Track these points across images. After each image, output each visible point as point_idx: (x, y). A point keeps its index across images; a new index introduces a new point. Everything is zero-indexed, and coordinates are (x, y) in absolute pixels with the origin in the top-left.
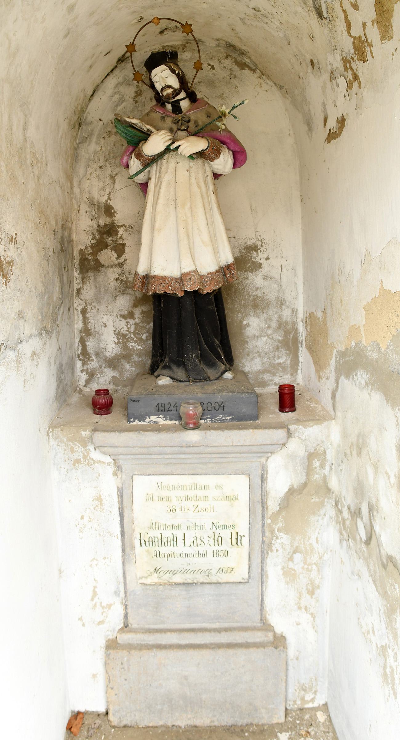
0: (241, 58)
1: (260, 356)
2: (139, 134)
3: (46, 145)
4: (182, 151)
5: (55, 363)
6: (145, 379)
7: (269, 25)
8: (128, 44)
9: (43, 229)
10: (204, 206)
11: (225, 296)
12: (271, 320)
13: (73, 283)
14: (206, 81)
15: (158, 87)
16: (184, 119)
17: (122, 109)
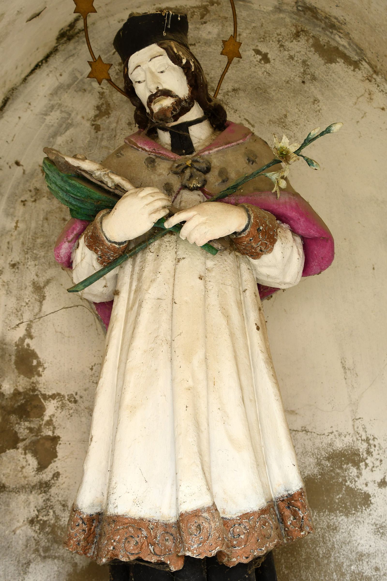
0: (327, 35)
2: (97, 194)
4: (190, 234)
10: (236, 357)
14: (250, 87)
16: (196, 165)
17: (67, 142)
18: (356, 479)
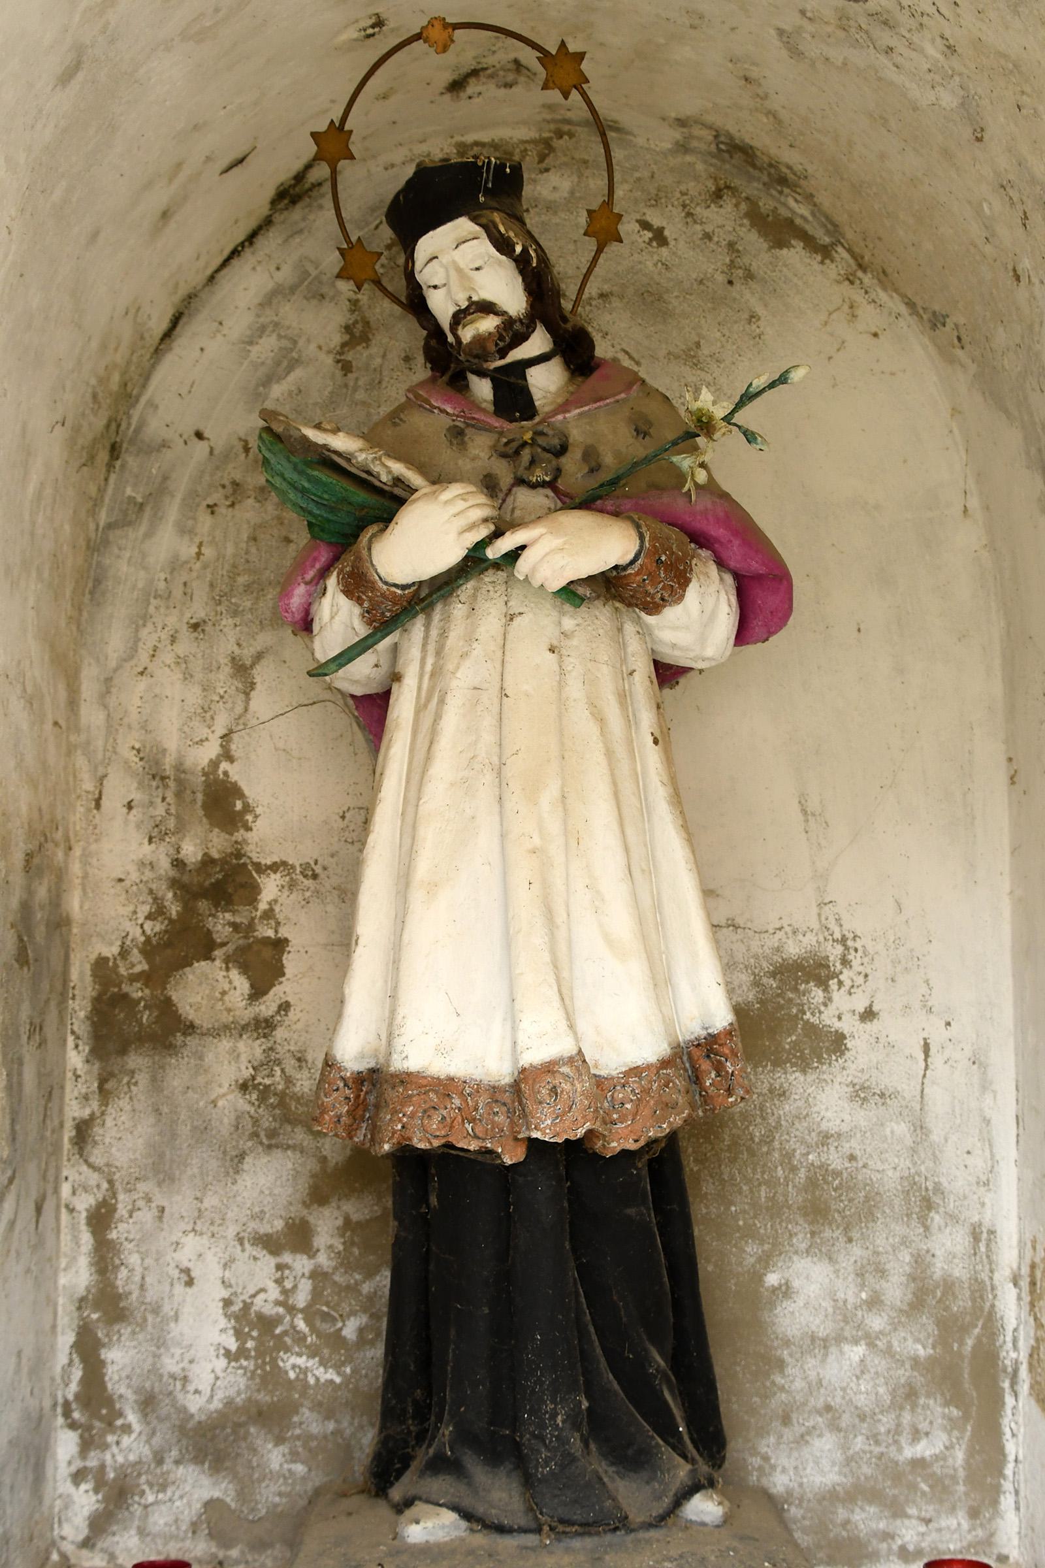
2: (360, 496)
4: (534, 569)
10: (616, 795)
15: (442, 306)
17: (290, 393)
18: (822, 1008)
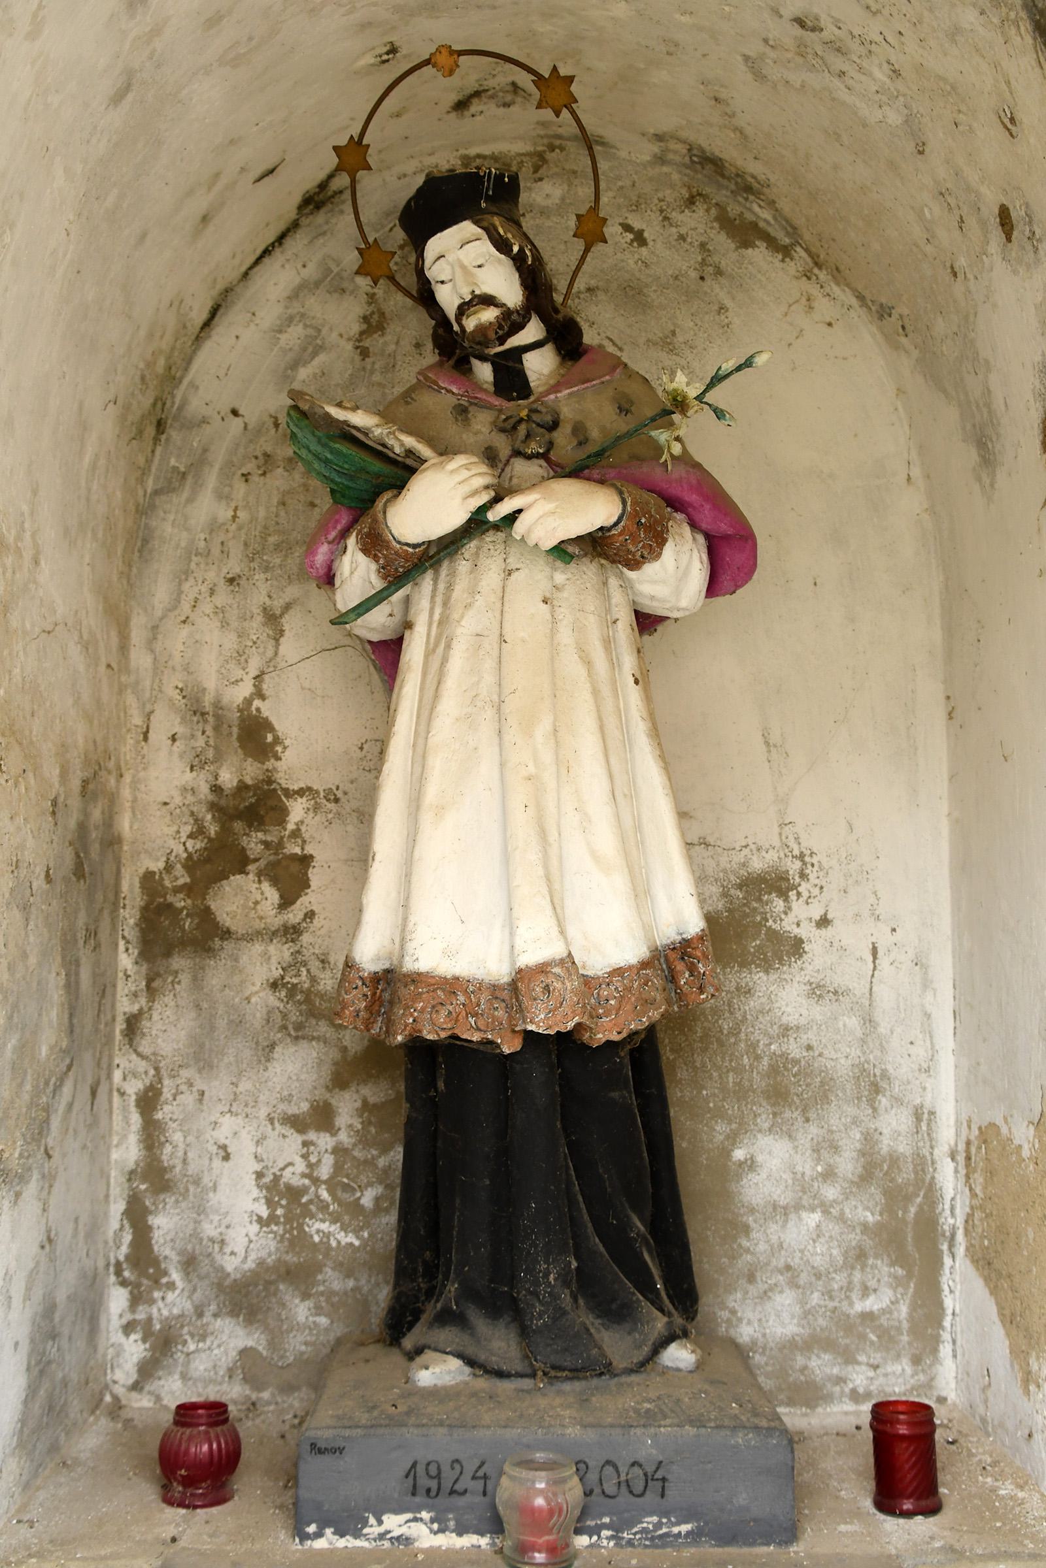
1: (794, 1284)
2: (376, 466)
3: (35, 493)
4: (529, 531)
5: (27, 1297)
6: (367, 1361)
7: (850, 82)
8: (343, 141)
9: (15, 793)
10: (602, 728)
11: (668, 1054)
12: (835, 1148)
13: (114, 995)
15: (448, 298)
16: (535, 417)
17: (315, 375)
18: (783, 916)
